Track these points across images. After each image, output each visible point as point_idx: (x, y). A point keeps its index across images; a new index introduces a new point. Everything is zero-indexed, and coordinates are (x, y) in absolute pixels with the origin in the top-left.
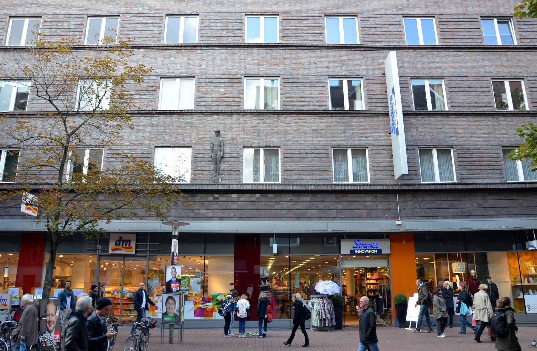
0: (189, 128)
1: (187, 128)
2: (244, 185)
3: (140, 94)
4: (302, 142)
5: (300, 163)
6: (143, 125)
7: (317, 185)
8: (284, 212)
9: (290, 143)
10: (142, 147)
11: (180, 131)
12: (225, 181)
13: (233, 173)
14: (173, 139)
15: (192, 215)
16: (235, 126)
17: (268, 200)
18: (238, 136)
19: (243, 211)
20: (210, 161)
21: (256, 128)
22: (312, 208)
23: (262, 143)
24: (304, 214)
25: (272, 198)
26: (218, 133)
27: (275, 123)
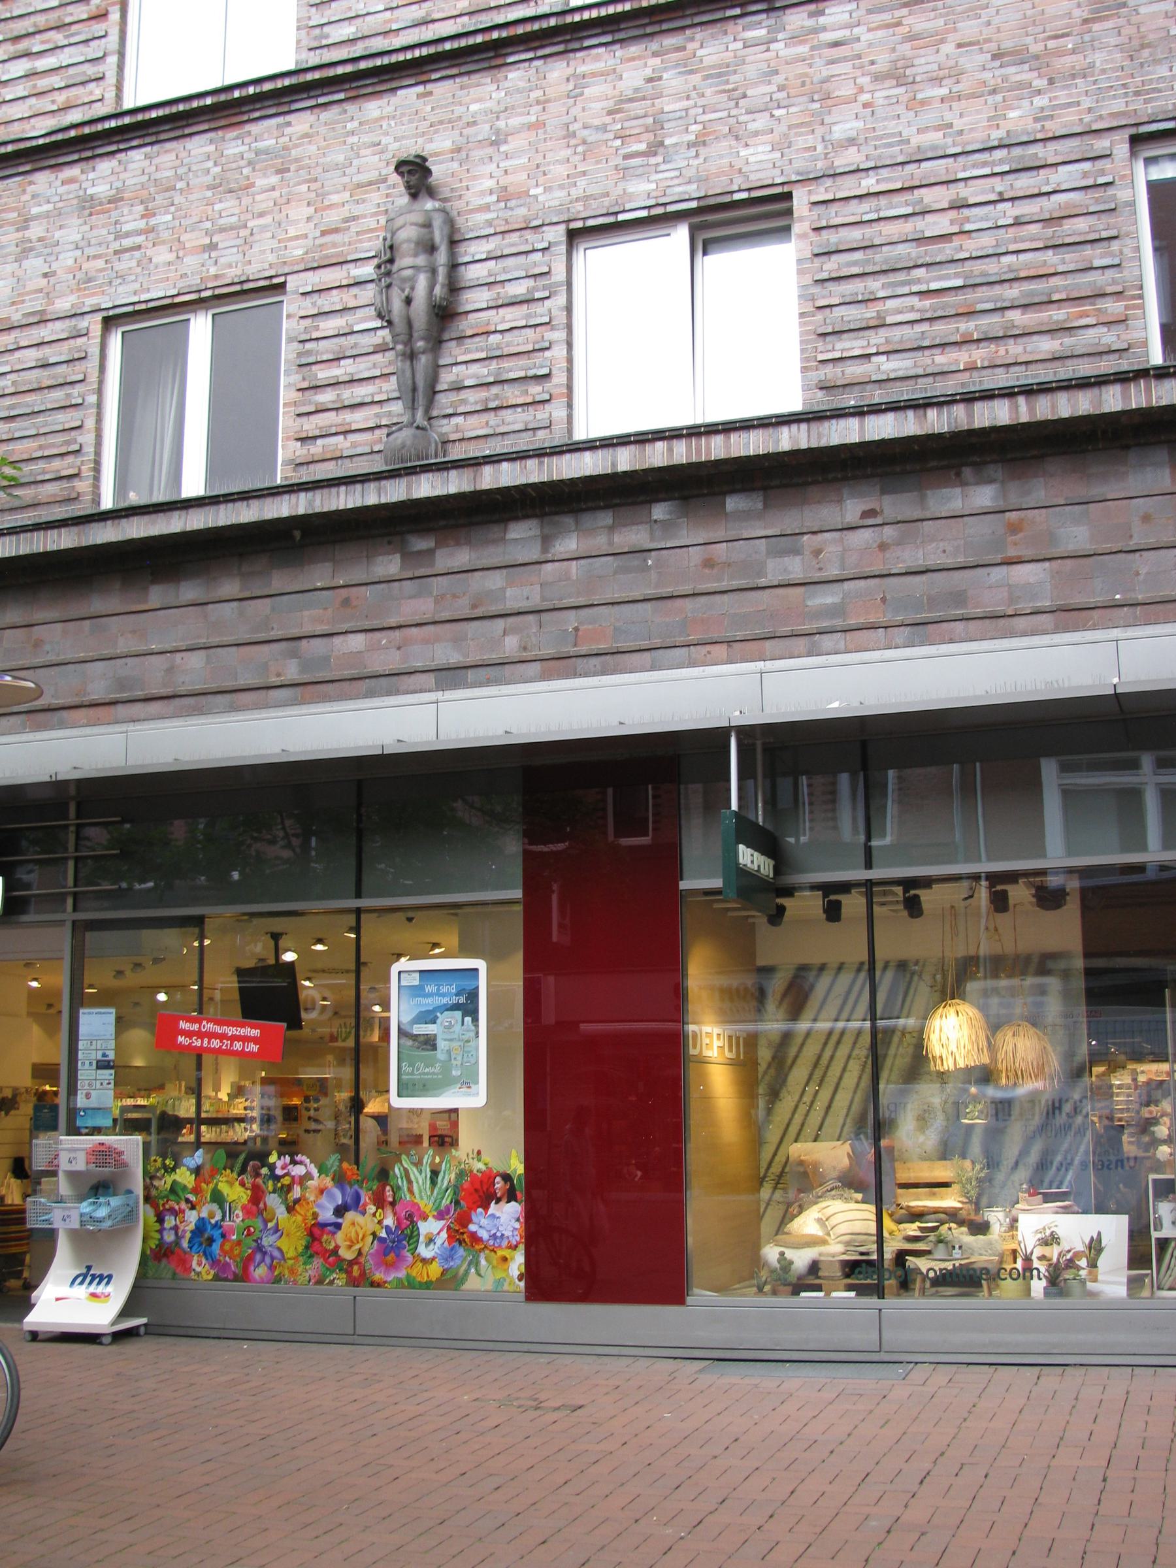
0: (274, 180)
1: (261, 182)
2: (591, 445)
3: (28, 55)
4: (935, 137)
5: (920, 273)
6: (47, 215)
7: (1029, 391)
8: (828, 598)
9: (851, 158)
10: (45, 333)
11: (228, 209)
12: (484, 434)
13: (513, 394)
14: (191, 262)
15: (292, 671)
16: (515, 122)
17: (720, 534)
18: (538, 170)
19: (571, 620)
20: (381, 349)
21: (637, 108)
22: (1012, 553)
23: (678, 191)
24: (959, 598)
25: (746, 516)
26: (416, 173)
27: (756, 56)
